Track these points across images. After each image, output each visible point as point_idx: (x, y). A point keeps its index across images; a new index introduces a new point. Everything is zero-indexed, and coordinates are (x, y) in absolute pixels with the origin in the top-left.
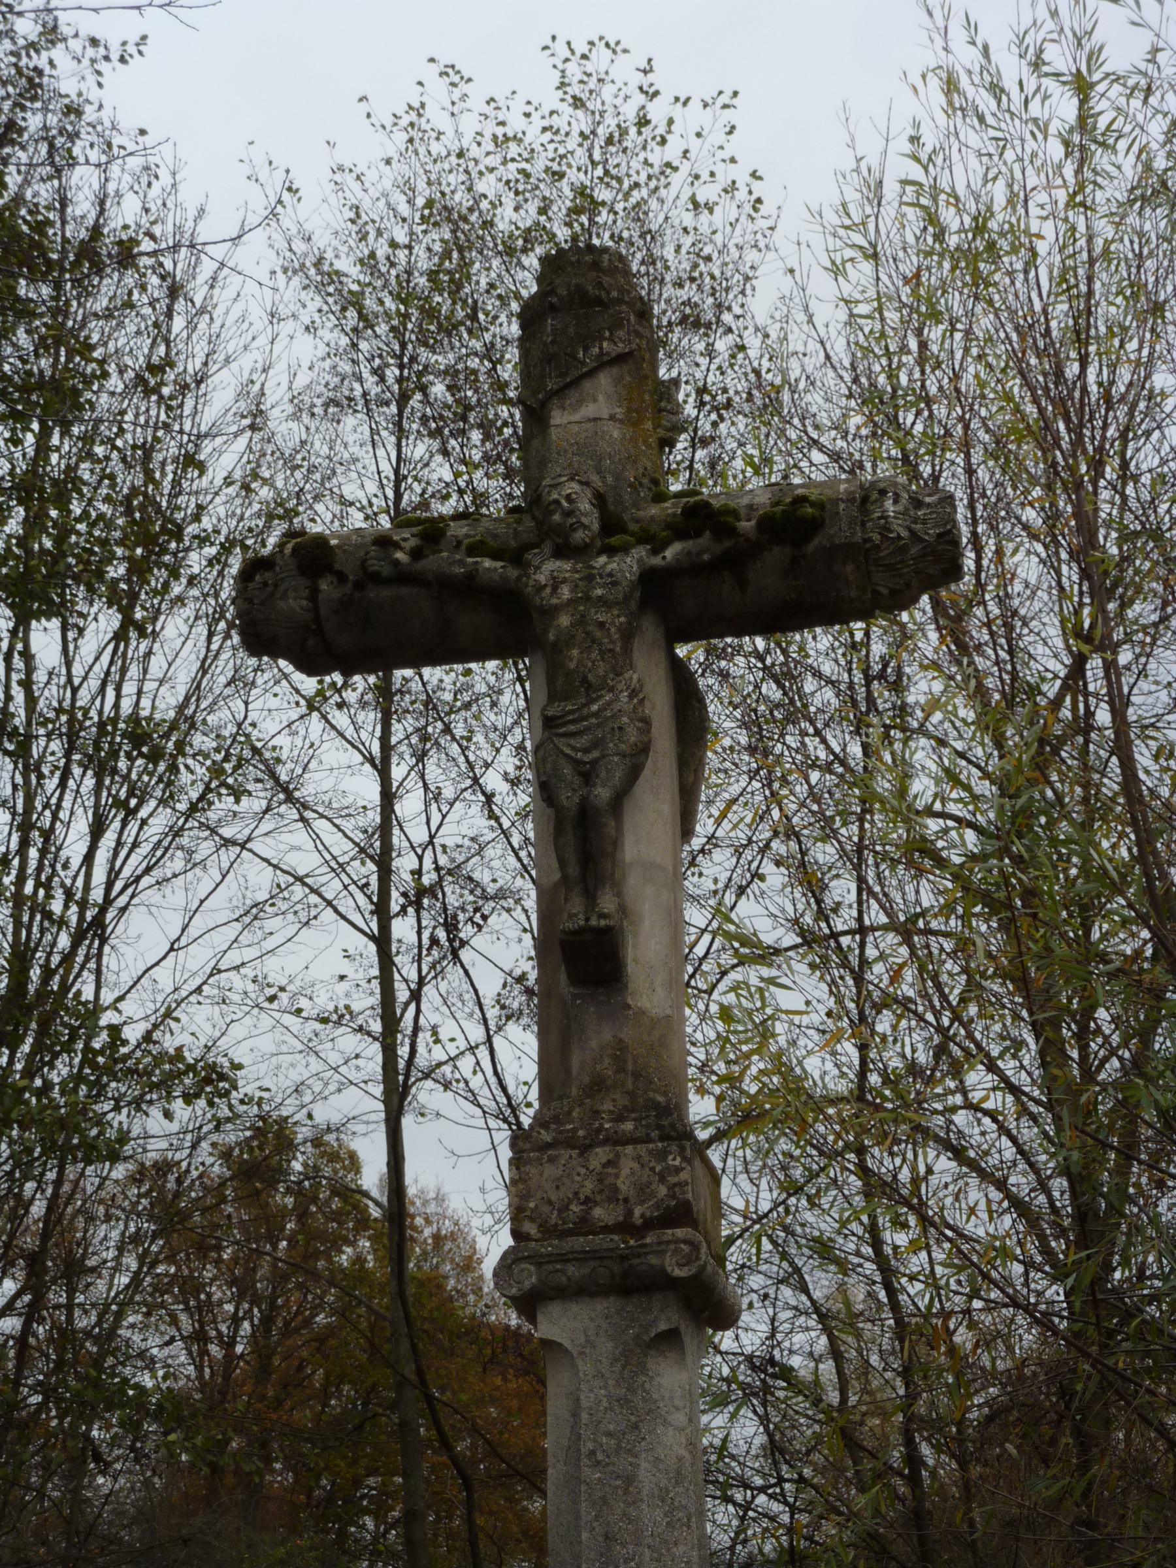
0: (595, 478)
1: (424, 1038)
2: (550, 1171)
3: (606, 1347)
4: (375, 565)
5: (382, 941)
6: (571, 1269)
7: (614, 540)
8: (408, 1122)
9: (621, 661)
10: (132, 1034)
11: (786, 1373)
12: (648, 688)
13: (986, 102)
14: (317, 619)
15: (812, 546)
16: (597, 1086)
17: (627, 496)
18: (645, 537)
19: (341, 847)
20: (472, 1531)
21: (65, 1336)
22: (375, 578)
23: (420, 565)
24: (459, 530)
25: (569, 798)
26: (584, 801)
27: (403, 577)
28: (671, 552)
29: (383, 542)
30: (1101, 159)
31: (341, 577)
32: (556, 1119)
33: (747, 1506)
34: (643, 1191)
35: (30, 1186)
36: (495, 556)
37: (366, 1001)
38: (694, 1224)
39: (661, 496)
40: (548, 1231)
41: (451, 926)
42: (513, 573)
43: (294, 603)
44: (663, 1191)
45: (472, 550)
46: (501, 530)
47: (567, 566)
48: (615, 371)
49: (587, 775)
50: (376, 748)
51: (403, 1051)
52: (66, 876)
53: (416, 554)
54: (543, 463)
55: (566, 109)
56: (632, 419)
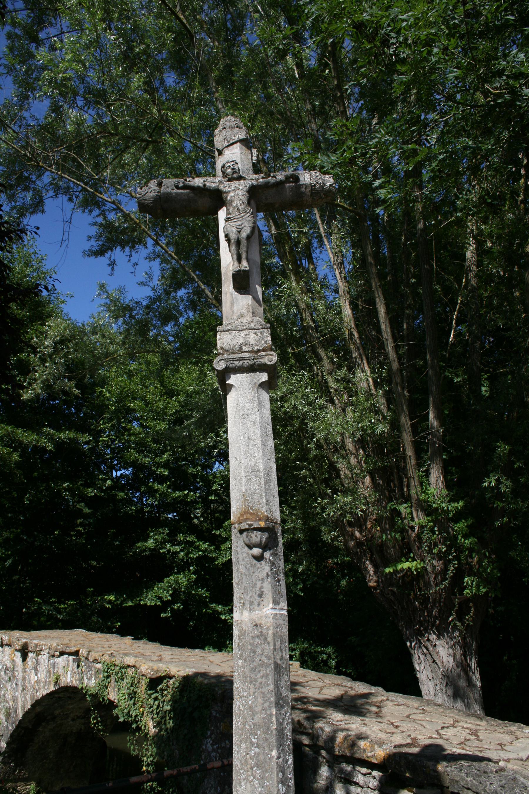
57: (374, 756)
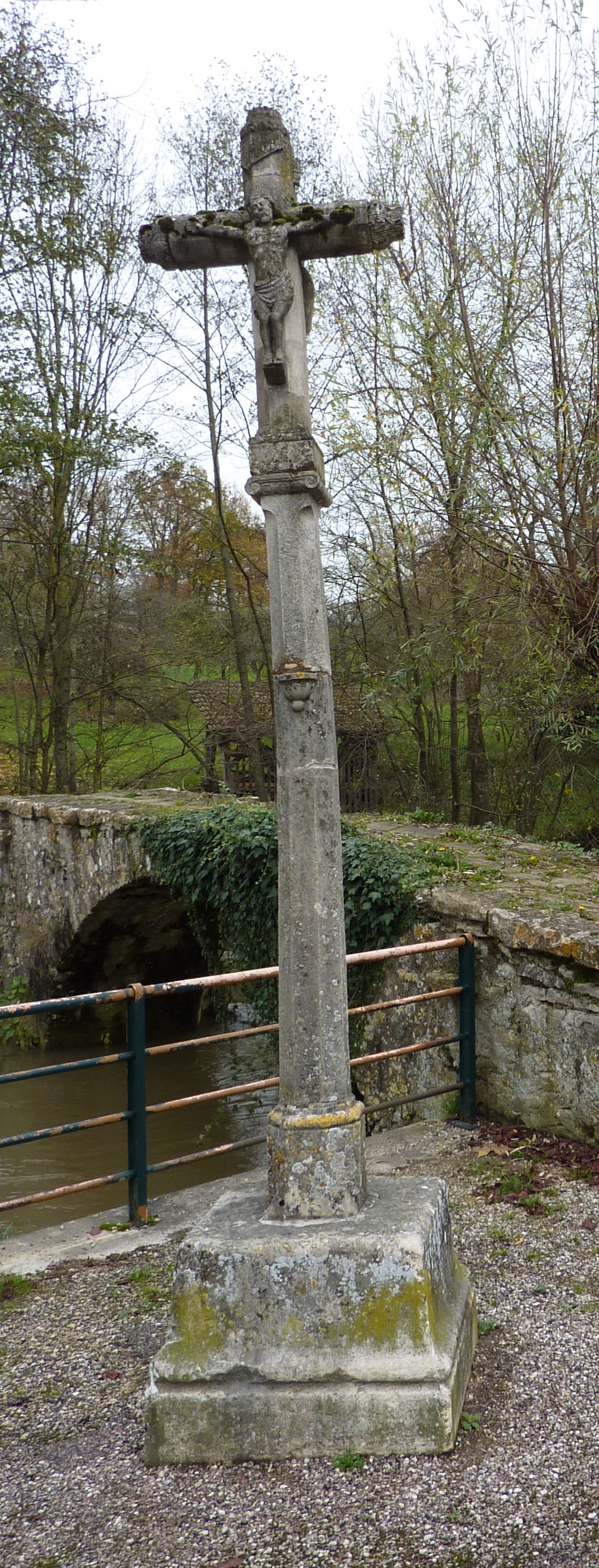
0: (270, 197)
1: (224, 424)
2: (263, 451)
3: (286, 512)
4: (189, 229)
5: (208, 391)
6: (272, 485)
7: (278, 220)
8: (220, 456)
9: (281, 266)
10: (120, 422)
11: (353, 540)
12: (292, 277)
13: (414, 74)
14: (169, 249)
15: (350, 225)
16: (279, 421)
17: (282, 203)
18: (289, 220)
19: (191, 357)
20: (250, 598)
21: (104, 530)
22: (190, 233)
23: (207, 228)
24: (220, 216)
25: (265, 317)
26: (270, 318)
27: (200, 233)
28: (299, 225)
29: (192, 219)
30: (454, 96)
31: (177, 233)
32: (265, 433)
33: (344, 585)
34: (296, 457)
35: (86, 479)
36: (234, 225)
37: (204, 413)
38: (315, 469)
39: (294, 205)
40: (263, 472)
41: (233, 387)
42: (241, 232)
43: (160, 242)
44: (303, 458)
45: (226, 223)
46: (236, 215)
47: (261, 229)
48: (276, 156)
49: (271, 308)
50: (203, 322)
51: (217, 430)
52: (91, 365)
53: (205, 224)
54: (251, 191)
55: (264, 80)
56: (283, 174)
57: (558, 947)
